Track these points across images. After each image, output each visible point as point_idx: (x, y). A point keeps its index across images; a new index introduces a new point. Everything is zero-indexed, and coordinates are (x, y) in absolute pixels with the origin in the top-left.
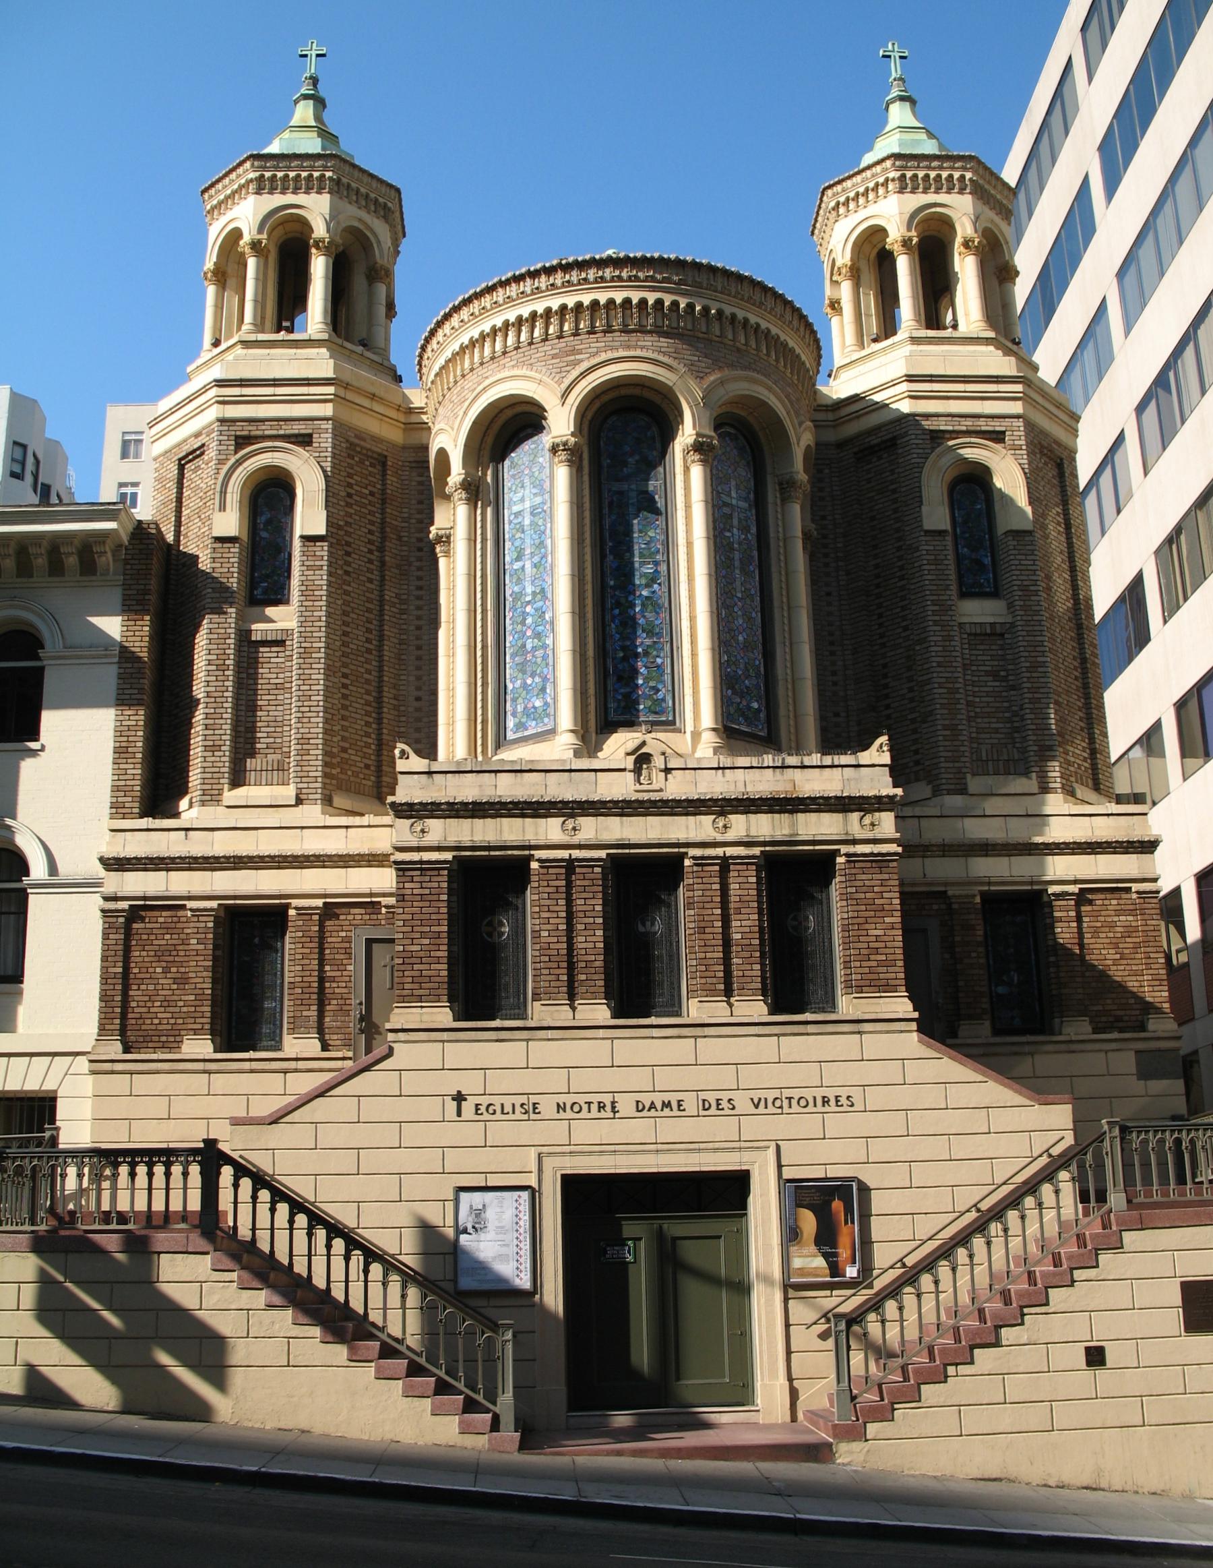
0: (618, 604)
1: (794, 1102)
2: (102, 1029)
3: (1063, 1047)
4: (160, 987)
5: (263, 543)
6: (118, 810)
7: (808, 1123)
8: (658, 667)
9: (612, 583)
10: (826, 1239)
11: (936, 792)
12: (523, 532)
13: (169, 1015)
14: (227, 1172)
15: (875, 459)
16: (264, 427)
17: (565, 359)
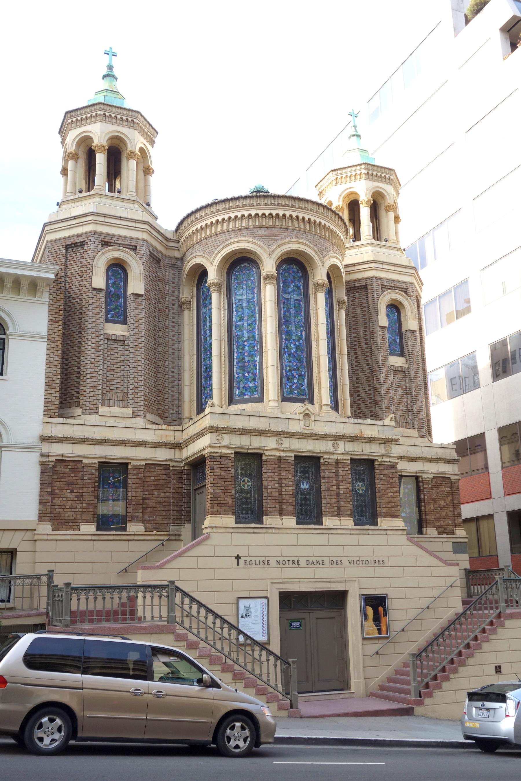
0: (287, 347)
1: (364, 562)
3: (428, 540)
4: (69, 499)
5: (111, 293)
6: (47, 413)
7: (369, 571)
8: (302, 375)
9: (285, 337)
10: (377, 619)
12: (243, 309)
13: (74, 513)
17: (271, 237)
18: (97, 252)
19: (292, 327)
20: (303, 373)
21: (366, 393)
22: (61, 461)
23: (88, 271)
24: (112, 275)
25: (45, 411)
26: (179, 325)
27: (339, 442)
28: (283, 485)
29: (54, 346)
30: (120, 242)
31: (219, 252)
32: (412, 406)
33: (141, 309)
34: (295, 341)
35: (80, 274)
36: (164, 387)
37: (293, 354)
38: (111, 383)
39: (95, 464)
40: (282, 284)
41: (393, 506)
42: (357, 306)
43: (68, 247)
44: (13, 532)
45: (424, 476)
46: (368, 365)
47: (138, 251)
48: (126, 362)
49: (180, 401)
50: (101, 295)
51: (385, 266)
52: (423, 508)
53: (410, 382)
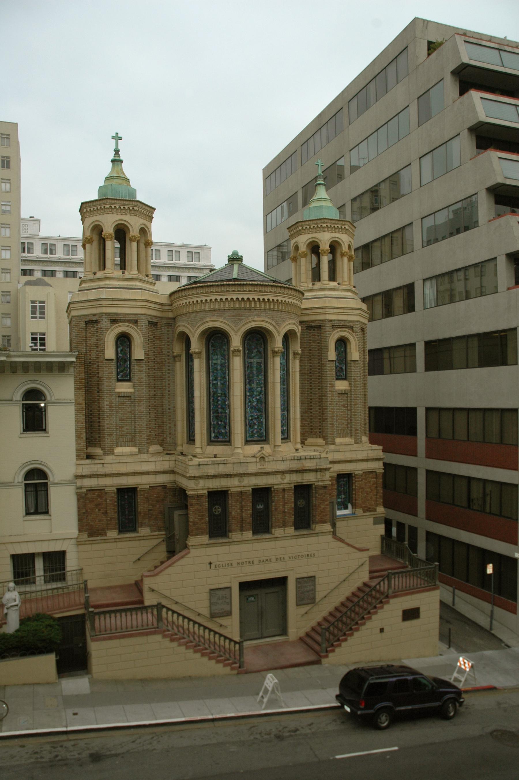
1: (300, 557)
2: (80, 530)
3: (356, 518)
5: (120, 358)
8: (261, 422)
9: (248, 394)
11: (327, 444)
12: (217, 370)
14: (164, 610)
15: (312, 330)
16: (120, 317)
17: (237, 317)
18: (107, 330)
19: (254, 385)
20: (262, 420)
21: (316, 411)
22: (91, 490)
23: (101, 345)
24: (121, 344)
25: (77, 456)
26: (174, 372)
27: (285, 475)
28: (243, 510)
29: (80, 408)
30: (124, 319)
31: (198, 327)
32: (351, 420)
33: (142, 371)
34: (256, 396)
35: (97, 345)
36: (163, 422)
37: (254, 406)
38: (123, 429)
39: (114, 490)
40: (247, 352)
41: (323, 516)
42: (313, 342)
43: (87, 323)
44: (62, 541)
45: (356, 473)
46: (319, 389)
47: (138, 324)
48: (133, 412)
49: (175, 431)
50: (112, 364)
51: (335, 310)
52: (354, 495)
53: (351, 401)
